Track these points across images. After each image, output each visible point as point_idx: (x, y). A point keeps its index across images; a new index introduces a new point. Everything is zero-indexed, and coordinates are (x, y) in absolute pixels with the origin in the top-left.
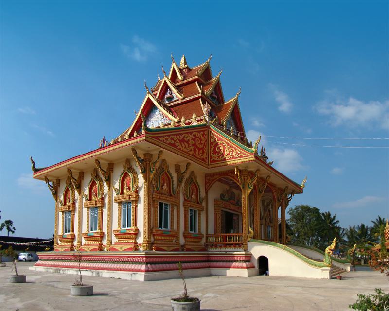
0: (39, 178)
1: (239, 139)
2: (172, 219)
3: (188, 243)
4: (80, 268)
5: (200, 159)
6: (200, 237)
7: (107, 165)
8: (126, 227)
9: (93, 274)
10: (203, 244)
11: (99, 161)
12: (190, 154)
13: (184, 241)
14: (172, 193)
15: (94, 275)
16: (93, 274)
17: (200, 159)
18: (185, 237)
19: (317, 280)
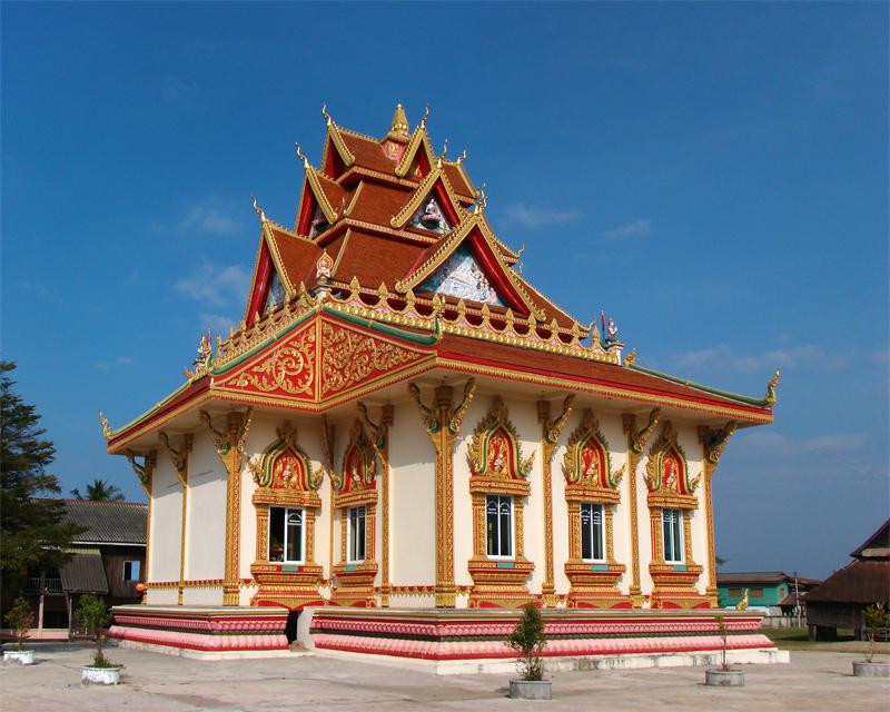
0: (118, 452)
1: (462, 310)
2: (344, 543)
3: (581, 589)
4: (724, 648)
5: (271, 392)
6: (614, 574)
7: (433, 391)
8: (589, 557)
9: (695, 661)
10: (703, 592)
11: (417, 388)
12: (239, 388)
13: (569, 585)
14: (516, 473)
15: (699, 662)
16: (695, 661)
17: (271, 392)
18: (569, 575)
19: (763, 665)
